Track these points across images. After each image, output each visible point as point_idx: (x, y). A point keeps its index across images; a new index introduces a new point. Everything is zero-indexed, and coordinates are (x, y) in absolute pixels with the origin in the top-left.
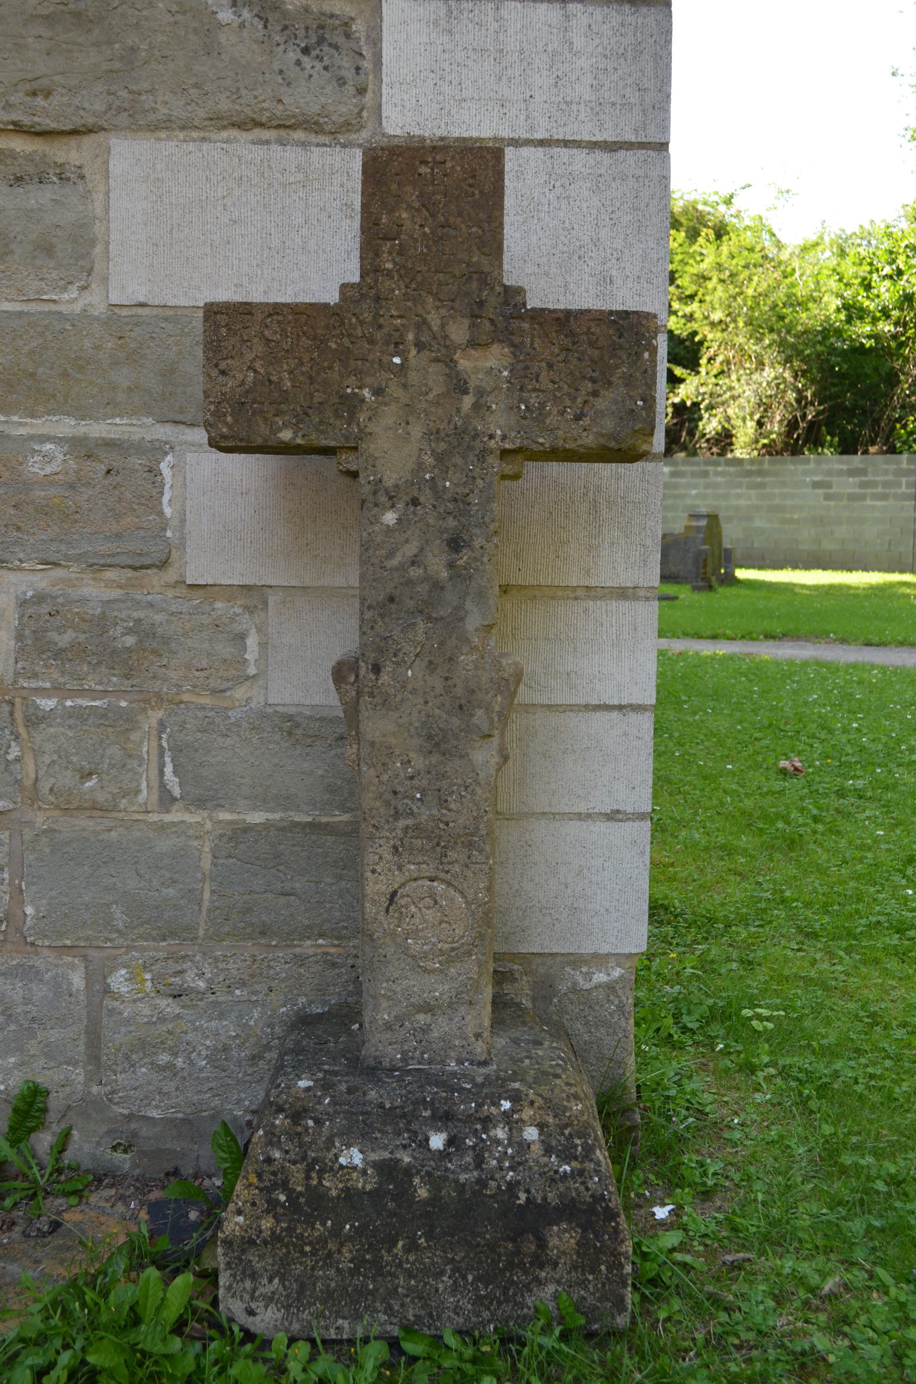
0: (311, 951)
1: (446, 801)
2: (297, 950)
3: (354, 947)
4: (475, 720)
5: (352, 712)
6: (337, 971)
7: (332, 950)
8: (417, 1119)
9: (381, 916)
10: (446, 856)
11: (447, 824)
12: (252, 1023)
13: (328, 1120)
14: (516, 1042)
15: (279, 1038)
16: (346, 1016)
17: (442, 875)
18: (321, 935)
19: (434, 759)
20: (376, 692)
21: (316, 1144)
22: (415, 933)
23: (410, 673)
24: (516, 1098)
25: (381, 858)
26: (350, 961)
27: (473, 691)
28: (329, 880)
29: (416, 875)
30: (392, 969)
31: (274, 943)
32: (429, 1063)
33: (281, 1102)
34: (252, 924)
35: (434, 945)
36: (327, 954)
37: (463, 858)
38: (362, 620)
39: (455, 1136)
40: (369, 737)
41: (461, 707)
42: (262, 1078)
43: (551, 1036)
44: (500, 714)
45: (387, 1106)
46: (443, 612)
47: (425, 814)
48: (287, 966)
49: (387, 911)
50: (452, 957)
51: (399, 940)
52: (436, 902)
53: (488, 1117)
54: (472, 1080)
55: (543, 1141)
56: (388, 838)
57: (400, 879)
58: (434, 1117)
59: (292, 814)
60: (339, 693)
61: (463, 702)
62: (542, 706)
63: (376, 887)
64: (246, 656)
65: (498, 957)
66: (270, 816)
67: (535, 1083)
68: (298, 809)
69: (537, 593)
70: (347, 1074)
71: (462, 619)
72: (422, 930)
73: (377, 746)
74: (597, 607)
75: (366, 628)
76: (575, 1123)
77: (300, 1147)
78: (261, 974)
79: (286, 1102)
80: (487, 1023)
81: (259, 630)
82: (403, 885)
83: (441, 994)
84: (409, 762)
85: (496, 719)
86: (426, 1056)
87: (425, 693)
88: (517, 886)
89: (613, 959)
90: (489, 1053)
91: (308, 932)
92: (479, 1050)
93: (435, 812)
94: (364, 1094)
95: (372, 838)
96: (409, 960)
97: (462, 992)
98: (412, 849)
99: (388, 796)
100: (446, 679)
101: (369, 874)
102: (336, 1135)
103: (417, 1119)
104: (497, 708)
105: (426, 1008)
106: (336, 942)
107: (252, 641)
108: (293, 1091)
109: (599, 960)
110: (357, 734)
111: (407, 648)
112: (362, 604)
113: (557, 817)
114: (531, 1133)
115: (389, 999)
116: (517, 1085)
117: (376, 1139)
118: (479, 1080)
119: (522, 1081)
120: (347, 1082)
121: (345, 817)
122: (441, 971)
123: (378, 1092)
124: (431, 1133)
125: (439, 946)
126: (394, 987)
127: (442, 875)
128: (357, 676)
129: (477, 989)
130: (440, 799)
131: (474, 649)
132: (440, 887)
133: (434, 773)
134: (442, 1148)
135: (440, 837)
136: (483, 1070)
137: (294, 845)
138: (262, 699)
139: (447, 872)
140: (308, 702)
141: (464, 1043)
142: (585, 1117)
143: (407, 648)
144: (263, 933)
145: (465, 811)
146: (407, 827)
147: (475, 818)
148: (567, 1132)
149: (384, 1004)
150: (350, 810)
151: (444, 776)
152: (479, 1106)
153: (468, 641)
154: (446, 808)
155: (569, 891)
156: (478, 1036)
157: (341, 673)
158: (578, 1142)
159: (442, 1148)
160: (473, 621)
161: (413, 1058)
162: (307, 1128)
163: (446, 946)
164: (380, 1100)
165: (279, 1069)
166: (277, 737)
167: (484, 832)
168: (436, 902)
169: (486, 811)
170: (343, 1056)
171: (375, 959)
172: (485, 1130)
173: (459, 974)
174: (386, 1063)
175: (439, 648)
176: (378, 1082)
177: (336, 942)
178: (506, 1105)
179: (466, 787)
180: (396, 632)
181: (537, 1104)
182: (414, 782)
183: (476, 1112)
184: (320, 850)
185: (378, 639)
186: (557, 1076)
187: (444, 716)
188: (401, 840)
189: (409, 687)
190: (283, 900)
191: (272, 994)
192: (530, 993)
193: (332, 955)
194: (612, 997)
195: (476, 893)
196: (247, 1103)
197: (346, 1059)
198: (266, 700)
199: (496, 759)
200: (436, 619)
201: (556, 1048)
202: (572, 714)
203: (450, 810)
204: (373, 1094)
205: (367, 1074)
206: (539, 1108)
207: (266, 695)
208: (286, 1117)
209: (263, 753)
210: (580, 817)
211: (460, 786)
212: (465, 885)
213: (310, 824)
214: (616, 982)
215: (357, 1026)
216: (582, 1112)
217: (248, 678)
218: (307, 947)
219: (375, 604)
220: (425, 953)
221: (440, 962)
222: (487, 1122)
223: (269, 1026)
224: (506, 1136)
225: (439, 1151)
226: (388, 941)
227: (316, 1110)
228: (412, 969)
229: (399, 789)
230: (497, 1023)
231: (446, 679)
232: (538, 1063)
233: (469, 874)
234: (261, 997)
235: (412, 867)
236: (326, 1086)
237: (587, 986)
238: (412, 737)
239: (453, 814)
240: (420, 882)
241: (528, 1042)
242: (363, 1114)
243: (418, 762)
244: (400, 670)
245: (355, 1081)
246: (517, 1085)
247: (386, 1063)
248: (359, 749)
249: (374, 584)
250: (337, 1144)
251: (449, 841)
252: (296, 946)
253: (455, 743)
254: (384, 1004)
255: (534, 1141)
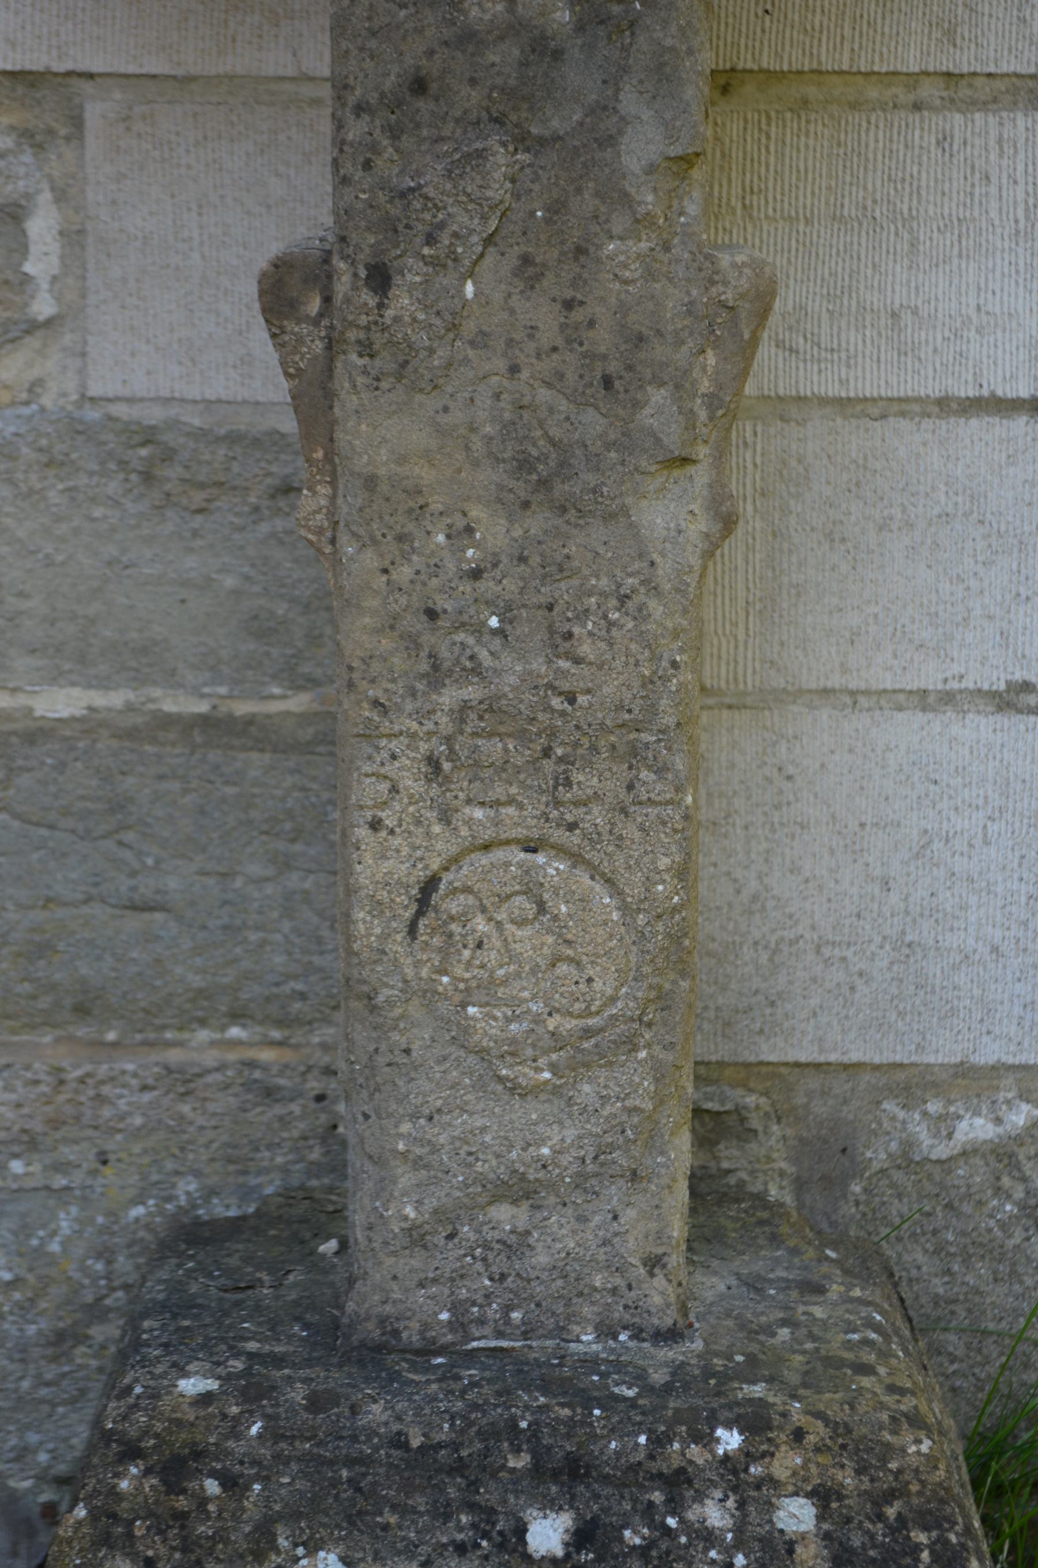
0: (210, 1058)
1: (569, 636)
2: (174, 1056)
3: (325, 1047)
4: (646, 417)
5: (315, 398)
6: (278, 1110)
7: (266, 1055)
8: (494, 1476)
9: (397, 945)
10: (568, 783)
11: (572, 699)
12: (55, 1247)
13: (257, 1478)
14: (755, 1285)
15: (126, 1287)
16: (306, 1218)
17: (559, 836)
18: (237, 1016)
19: (537, 523)
20: (378, 339)
21: (226, 1541)
22: (487, 991)
23: (469, 289)
24: (755, 1422)
25: (394, 789)
26: (314, 1085)
27: (641, 338)
28: (255, 869)
29: (488, 835)
30: (427, 1086)
31: (111, 1036)
32: (525, 1335)
33: (133, 1433)
34: (53, 987)
35: (537, 1020)
36: (252, 1064)
37: (613, 787)
38: (340, 144)
39: (595, 1520)
40: (361, 463)
41: (607, 382)
42: (83, 1392)
43: (846, 1272)
44: (712, 401)
45: (416, 1442)
46: (560, 121)
47: (512, 672)
48: (147, 1097)
49: (412, 930)
50: (585, 1052)
51: (444, 1008)
52: (542, 907)
53: (681, 1471)
54: (640, 1378)
55: (827, 1536)
56: (413, 736)
57: (445, 846)
58: (537, 1471)
59: (157, 692)
60: (280, 346)
61: (613, 367)
62: (824, 401)
63: (383, 867)
64: (28, 268)
65: (707, 1073)
66: (99, 699)
67: (805, 1385)
68: (171, 679)
69: (812, 91)
70: (309, 1363)
71: (610, 141)
72: (505, 982)
73: (384, 488)
74: (977, 130)
75: (348, 163)
76: (914, 1488)
77: (185, 1550)
78: (77, 1118)
79: (145, 1433)
80: (678, 1229)
81: (61, 196)
82: (454, 861)
83: (555, 1152)
84: (469, 530)
85: (703, 415)
86: (516, 1315)
87: (510, 342)
88: (753, 885)
89: (1008, 1081)
90: (684, 1310)
91: (201, 1008)
92: (657, 1299)
93: (539, 665)
94: (354, 1410)
95: (370, 735)
96: (472, 1060)
97: (612, 1147)
98: (477, 764)
99: (416, 623)
100: (569, 305)
101: (362, 832)
102: (280, 1517)
103: (494, 1476)
104: (705, 386)
105: (519, 1189)
106: (276, 1034)
107: (42, 226)
108: (165, 1404)
109: (973, 1081)
110: (328, 458)
111: (462, 219)
112: (339, 99)
113: (863, 701)
114: (797, 1515)
115: (418, 1164)
116: (758, 1390)
117: (386, 1527)
118: (659, 1377)
119: (770, 1380)
120: (306, 1381)
121: (299, 702)
122: (556, 1091)
123: (389, 1406)
124: (531, 1514)
125: (551, 1024)
126: (431, 1131)
127: (559, 836)
128: (327, 300)
129: (652, 1139)
130: (551, 630)
131: (644, 222)
132: (552, 868)
133: (535, 560)
134: (560, 1553)
135: (553, 734)
136: (668, 1353)
137: (161, 777)
138: (71, 385)
139: (572, 827)
140: (194, 392)
141: (618, 1281)
142: (941, 1473)
143: (462, 219)
144: (81, 1011)
145: (618, 664)
146: (465, 707)
147: (647, 682)
148: (891, 1512)
149: (406, 1179)
150: (311, 683)
151: (562, 569)
152: (659, 1441)
153: (626, 200)
154: (568, 656)
155: (894, 898)
156: (654, 1263)
157: (285, 290)
158: (921, 1537)
159: (560, 1553)
160: (641, 147)
161: (481, 1322)
162: (203, 1501)
163: (570, 1024)
164: (395, 1427)
165: (130, 1351)
166: (113, 487)
167: (670, 720)
168: (542, 907)
169: (674, 664)
170: (297, 1319)
171: (381, 1060)
172: (674, 1505)
173: (604, 1099)
174: (411, 1335)
175: (548, 221)
176: (391, 1383)
177: (276, 1034)
178: (730, 1440)
179: (624, 599)
180: (433, 178)
181: (811, 1439)
182: (482, 585)
183: (651, 1457)
184: (230, 790)
185: (382, 197)
186: (867, 1370)
187: (564, 406)
188: (449, 740)
189: (469, 327)
190: (134, 922)
191: (108, 1171)
192: (791, 1169)
193: (265, 1068)
194: (1006, 1181)
195: (649, 883)
196: (43, 1457)
197: (306, 1326)
198: (83, 386)
199: (701, 525)
200: (542, 141)
201: (860, 1301)
202: (903, 424)
203: (578, 661)
204: (376, 1412)
205: (361, 1363)
206: (817, 1450)
207: (82, 372)
208: (148, 1472)
209: (76, 531)
210: (924, 700)
211: (604, 595)
212: (620, 859)
213: (204, 721)
214: (1018, 1140)
215: (332, 1245)
216: (931, 1460)
217: (33, 327)
218: (201, 1046)
219: (373, 98)
220: (513, 1041)
221: (553, 1067)
222: (680, 1484)
223: (99, 1256)
224: (728, 1522)
225: (554, 1560)
226: (415, 1009)
227: (228, 1453)
228: (479, 1086)
229: (442, 603)
230: (704, 1240)
231: (569, 305)
232: (814, 1338)
233: (631, 831)
234: (78, 1178)
235: (479, 814)
236: (253, 1391)
237: (941, 1151)
238: (476, 464)
239: (585, 670)
240: (499, 855)
241: (786, 1286)
242: (350, 1462)
243: (495, 532)
244: (446, 280)
245: (334, 1379)
246: (758, 1390)
247: (411, 1335)
248: (333, 498)
249: (372, 44)
250: (283, 1542)
251: (576, 745)
252: (169, 1044)
253: (591, 479)
254: (406, 1179)
255: (803, 1536)
